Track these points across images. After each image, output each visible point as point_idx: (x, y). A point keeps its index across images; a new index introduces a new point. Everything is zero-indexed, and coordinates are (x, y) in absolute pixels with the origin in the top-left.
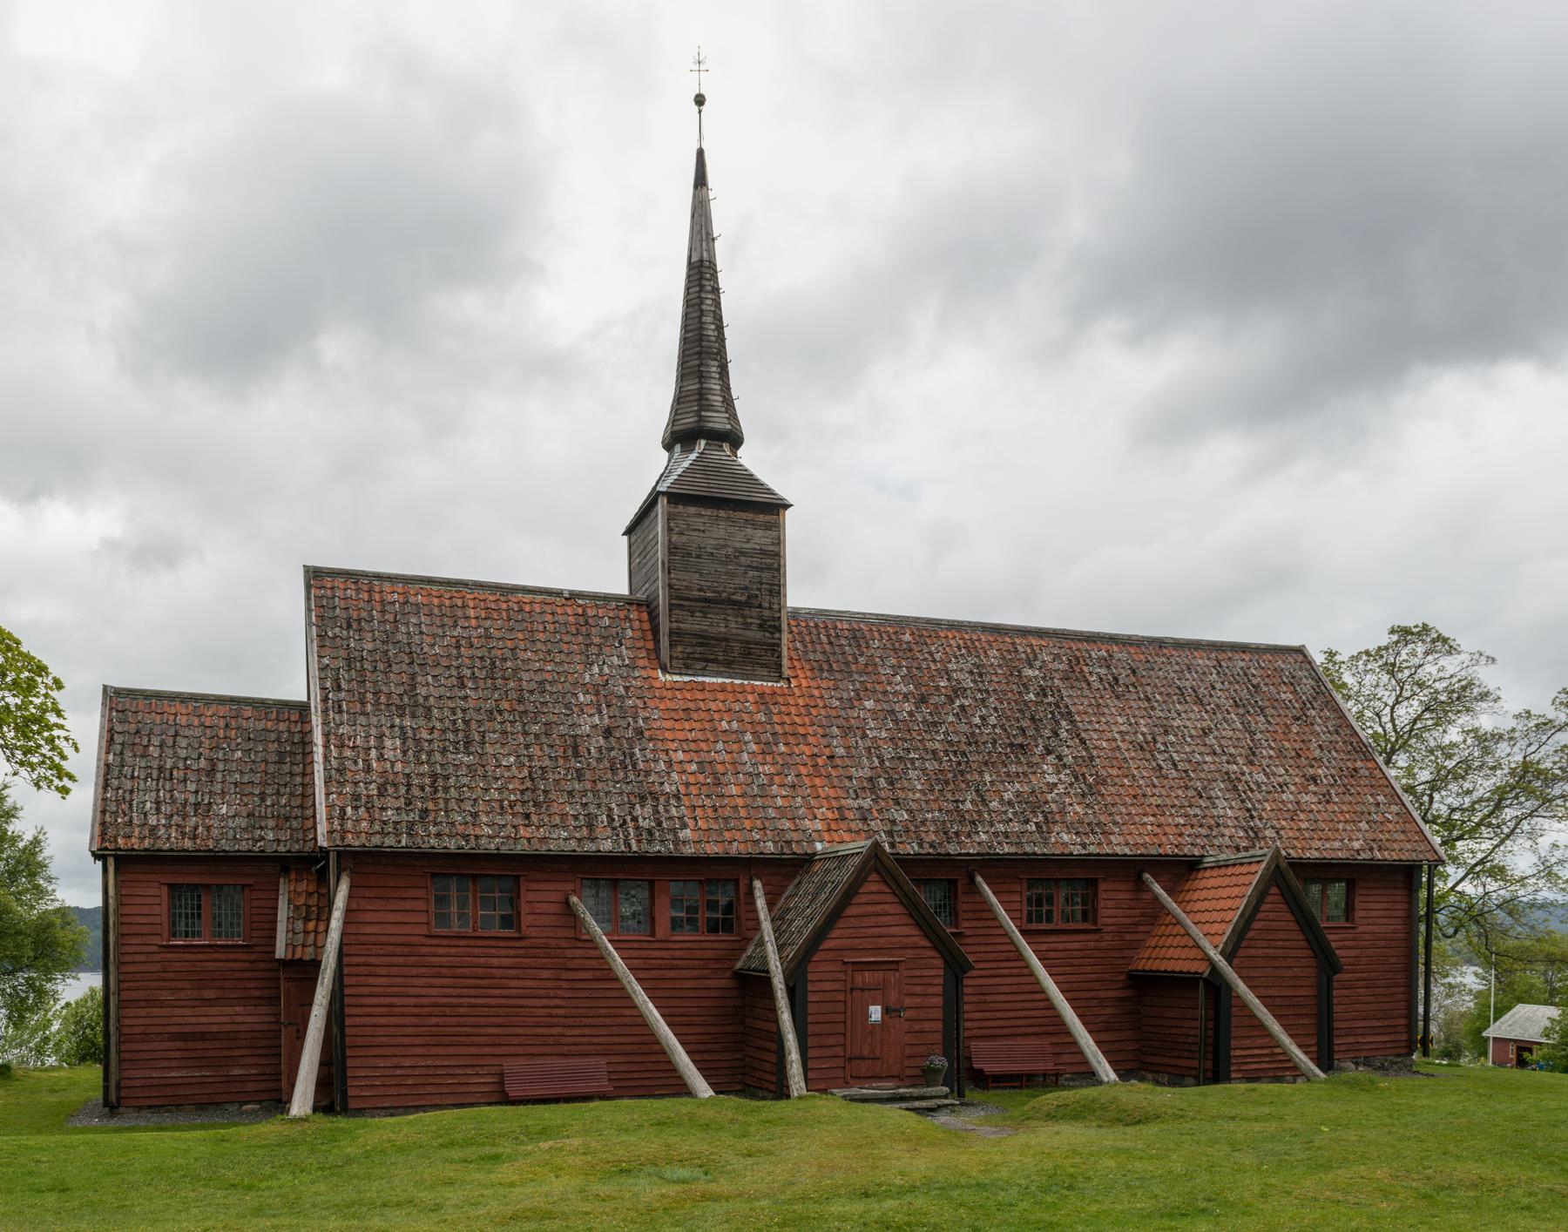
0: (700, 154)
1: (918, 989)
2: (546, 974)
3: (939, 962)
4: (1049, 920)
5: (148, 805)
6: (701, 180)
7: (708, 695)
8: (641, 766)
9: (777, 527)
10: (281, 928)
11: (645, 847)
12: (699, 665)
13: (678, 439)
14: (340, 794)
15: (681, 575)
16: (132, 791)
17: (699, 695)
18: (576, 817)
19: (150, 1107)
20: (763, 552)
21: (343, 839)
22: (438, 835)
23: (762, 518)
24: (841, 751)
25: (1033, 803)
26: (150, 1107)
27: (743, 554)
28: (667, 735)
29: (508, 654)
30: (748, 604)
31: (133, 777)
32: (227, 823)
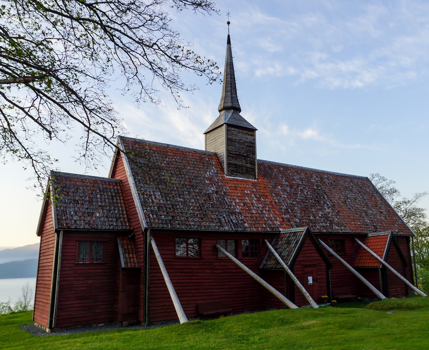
0: (229, 36)
1: (320, 273)
2: (209, 271)
3: (324, 265)
5: (72, 213)
6: (229, 42)
7: (239, 183)
8: (228, 204)
9: (254, 135)
10: (122, 256)
11: (237, 229)
12: (235, 174)
13: (224, 109)
14: (146, 210)
15: (231, 147)
16: (66, 208)
17: (236, 183)
18: (215, 219)
19: (66, 327)
20: (251, 143)
21: (151, 225)
22: (179, 224)
23: (250, 133)
24: (277, 201)
25: (326, 217)
26: (66, 327)
27: (246, 142)
28: (232, 194)
29: (183, 167)
30: (247, 157)
31: (65, 203)
32: (100, 219)
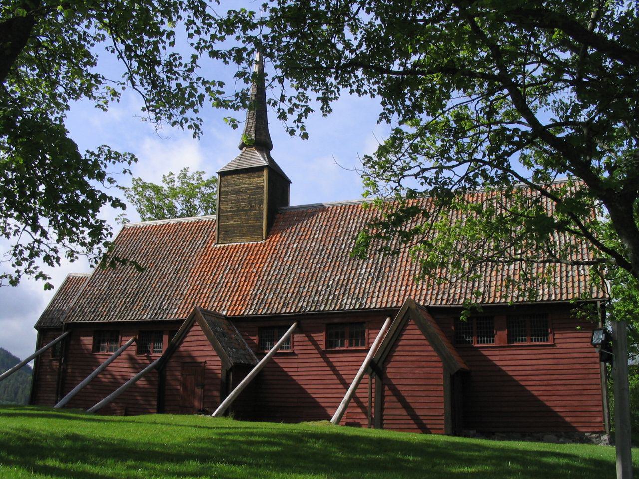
4: (493, 342)
27: (248, 189)
